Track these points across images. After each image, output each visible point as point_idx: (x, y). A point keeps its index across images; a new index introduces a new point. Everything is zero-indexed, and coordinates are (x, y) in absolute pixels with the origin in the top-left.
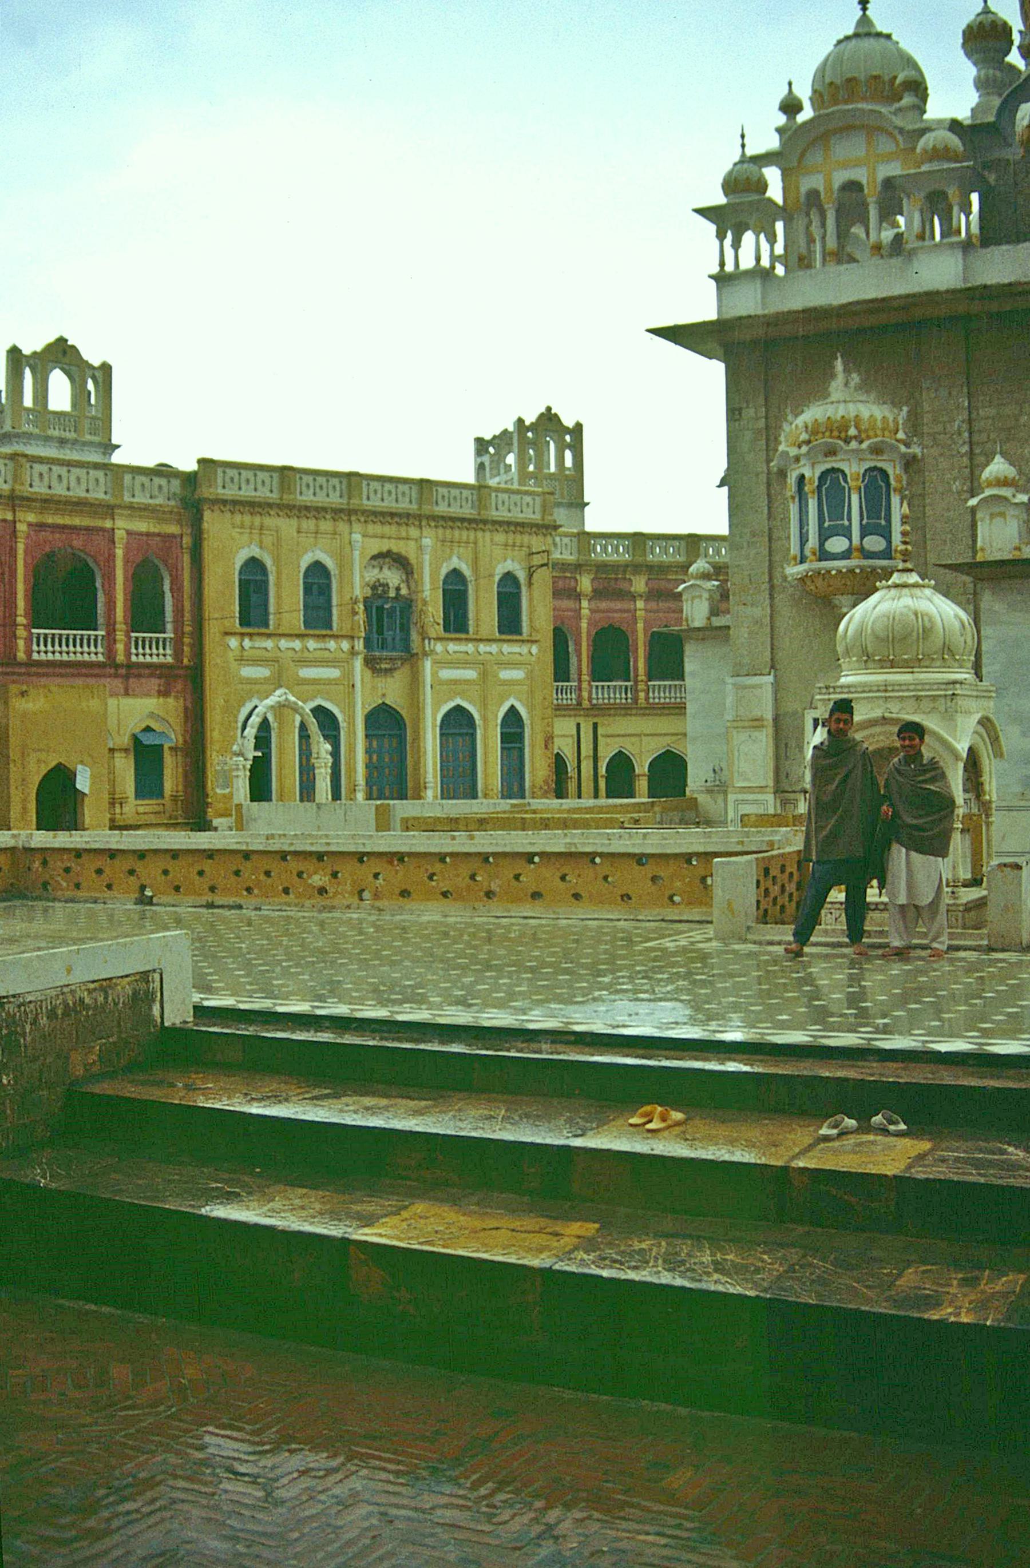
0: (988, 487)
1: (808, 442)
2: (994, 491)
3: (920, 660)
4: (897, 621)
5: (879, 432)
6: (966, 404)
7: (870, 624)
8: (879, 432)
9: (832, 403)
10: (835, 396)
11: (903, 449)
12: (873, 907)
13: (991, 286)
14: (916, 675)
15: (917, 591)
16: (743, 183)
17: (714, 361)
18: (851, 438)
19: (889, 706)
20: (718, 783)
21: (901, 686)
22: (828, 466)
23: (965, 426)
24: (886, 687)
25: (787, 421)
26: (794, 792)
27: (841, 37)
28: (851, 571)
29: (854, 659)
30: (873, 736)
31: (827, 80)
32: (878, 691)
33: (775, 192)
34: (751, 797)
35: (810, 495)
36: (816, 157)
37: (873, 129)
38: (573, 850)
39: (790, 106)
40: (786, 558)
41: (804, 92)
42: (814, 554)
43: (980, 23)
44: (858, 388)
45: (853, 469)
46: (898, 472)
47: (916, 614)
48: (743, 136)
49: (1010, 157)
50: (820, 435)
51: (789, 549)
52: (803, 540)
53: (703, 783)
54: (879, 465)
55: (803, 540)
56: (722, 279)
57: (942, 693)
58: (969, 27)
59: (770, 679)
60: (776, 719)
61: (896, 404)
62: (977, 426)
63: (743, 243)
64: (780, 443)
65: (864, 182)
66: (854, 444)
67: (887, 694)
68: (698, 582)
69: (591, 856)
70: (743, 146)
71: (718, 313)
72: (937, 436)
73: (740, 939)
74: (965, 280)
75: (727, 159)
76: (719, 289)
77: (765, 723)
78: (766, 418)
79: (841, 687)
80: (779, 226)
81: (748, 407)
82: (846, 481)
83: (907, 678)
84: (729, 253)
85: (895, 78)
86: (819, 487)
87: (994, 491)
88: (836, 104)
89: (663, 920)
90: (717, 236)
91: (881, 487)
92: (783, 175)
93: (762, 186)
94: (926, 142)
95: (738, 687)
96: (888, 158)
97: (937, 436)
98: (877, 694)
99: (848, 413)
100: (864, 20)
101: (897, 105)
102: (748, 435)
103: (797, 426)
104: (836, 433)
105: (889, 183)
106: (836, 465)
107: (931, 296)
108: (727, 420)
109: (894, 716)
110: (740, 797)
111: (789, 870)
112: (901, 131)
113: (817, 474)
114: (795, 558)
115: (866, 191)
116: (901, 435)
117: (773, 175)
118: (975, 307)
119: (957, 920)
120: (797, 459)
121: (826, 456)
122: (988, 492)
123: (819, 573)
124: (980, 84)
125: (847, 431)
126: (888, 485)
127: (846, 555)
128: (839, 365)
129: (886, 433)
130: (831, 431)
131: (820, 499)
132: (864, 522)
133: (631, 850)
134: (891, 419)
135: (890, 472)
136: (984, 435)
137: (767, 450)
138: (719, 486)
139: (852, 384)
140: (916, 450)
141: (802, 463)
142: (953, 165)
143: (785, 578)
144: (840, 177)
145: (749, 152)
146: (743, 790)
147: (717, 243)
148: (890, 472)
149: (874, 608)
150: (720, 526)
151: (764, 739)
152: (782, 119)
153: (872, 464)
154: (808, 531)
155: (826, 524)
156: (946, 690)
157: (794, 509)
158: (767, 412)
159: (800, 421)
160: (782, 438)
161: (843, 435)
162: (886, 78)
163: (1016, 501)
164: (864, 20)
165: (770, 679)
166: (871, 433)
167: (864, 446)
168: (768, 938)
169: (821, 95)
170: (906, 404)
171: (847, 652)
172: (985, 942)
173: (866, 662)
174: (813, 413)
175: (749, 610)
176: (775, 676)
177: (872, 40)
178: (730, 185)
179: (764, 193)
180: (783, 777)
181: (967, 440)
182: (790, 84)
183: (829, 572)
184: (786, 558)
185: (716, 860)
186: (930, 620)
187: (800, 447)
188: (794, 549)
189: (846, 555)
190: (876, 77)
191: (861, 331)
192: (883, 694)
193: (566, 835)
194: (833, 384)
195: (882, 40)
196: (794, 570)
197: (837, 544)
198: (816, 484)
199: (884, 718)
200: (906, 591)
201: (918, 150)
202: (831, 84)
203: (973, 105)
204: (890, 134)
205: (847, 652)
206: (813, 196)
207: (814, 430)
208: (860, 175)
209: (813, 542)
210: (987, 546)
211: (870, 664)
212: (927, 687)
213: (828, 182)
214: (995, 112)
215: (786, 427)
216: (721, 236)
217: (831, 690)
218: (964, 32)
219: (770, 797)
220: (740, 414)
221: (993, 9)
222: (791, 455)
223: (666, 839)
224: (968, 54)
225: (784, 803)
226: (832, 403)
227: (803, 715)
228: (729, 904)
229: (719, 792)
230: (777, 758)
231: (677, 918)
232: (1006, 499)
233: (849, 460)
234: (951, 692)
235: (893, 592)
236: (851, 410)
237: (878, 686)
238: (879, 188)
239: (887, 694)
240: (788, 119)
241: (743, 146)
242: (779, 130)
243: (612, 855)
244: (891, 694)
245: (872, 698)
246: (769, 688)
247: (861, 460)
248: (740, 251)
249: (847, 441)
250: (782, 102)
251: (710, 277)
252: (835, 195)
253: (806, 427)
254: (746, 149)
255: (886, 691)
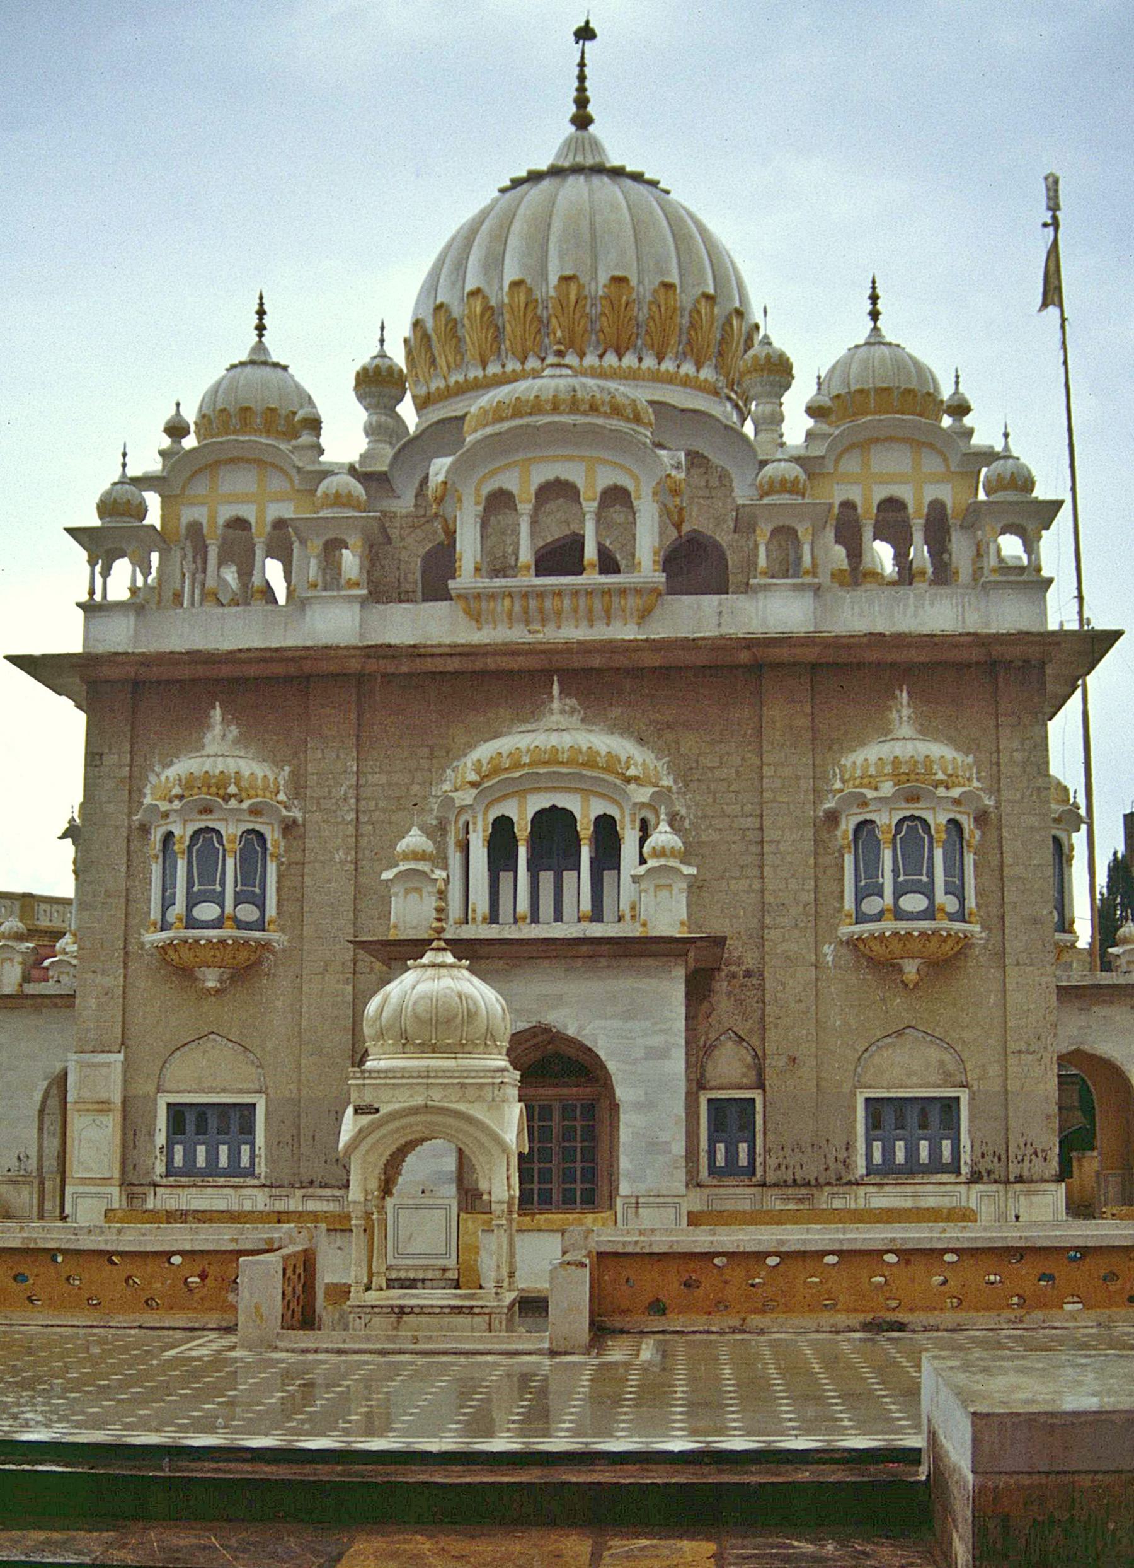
0: (402, 860)
1: (181, 797)
2: (412, 865)
3: (463, 1045)
4: (440, 1003)
5: (260, 792)
6: (355, 769)
7: (411, 1003)
8: (260, 792)
9: (208, 756)
10: (209, 750)
11: (284, 812)
12: (409, 1310)
13: (395, 646)
14: (460, 1061)
15: (455, 971)
16: (120, 506)
17: (64, 698)
18: (230, 796)
19: (430, 1093)
20: (22, 1173)
21: (445, 1073)
22: (202, 825)
23: (352, 793)
24: (427, 1073)
25: (153, 771)
26: (142, 1185)
27: (236, 362)
28: (222, 942)
29: (390, 1042)
30: (411, 1126)
31: (219, 406)
32: (419, 1077)
33: (154, 517)
34: (93, 1189)
35: (179, 855)
36: (201, 488)
37: (262, 463)
38: (32, 1246)
39: (176, 430)
40: (145, 924)
41: (190, 415)
42: (180, 920)
43: (377, 366)
44: (236, 742)
45: (231, 830)
46: (276, 837)
47: (460, 997)
48: (124, 455)
49: (398, 510)
50: (196, 790)
51: (149, 913)
52: (167, 903)
53: (5, 1173)
54: (258, 827)
55: (167, 903)
56: (89, 608)
57: (490, 1080)
58: (365, 370)
59: (121, 1056)
60: (125, 1101)
61: (278, 764)
62: (365, 793)
63: (112, 572)
64: (145, 795)
65: (253, 521)
66: (233, 803)
67: (430, 1081)
68: (10, 943)
69: (52, 1253)
70: (124, 465)
71: (84, 646)
72: (322, 801)
73: (270, 1346)
74: (362, 636)
75: (106, 477)
76: (86, 618)
77: (112, 1106)
78: (131, 766)
79: (370, 1072)
80: (155, 557)
81: (110, 752)
82: (221, 843)
83: (451, 1063)
84: (99, 580)
85: (295, 413)
86: (190, 847)
87: (412, 865)
88: (227, 434)
89: (140, 1327)
90: (89, 562)
91: (256, 852)
92: (162, 502)
93: (142, 511)
94: (328, 485)
95: (83, 1065)
96: (279, 498)
97: (322, 801)
98: (420, 1081)
99: (228, 767)
100: (260, 347)
101: (294, 443)
102: (110, 784)
103: (167, 778)
104: (213, 790)
105: (280, 524)
106: (211, 825)
107: (327, 651)
108: (86, 765)
109: (437, 1104)
110: (80, 1189)
111: (298, 1271)
112: (299, 470)
113: (189, 832)
114: (155, 924)
115: (253, 531)
116: (282, 797)
117: (153, 500)
118: (372, 666)
119: (501, 1323)
120: (166, 815)
121: (200, 812)
122: (403, 867)
123: (186, 942)
124: (371, 430)
125: (226, 789)
126: (265, 849)
127: (218, 924)
128: (217, 714)
129: (268, 794)
130: (209, 787)
131: (190, 863)
132: (238, 889)
133: (103, 1247)
134: (272, 779)
135: (268, 836)
136: (372, 805)
137: (129, 802)
138: (60, 838)
139: (230, 737)
140: (297, 814)
141: (171, 819)
142: (356, 514)
143: (142, 946)
144: (226, 513)
145: (132, 472)
146: (84, 1181)
147: (88, 568)
148: (269, 837)
149: (414, 987)
150: (64, 886)
151: (111, 1123)
152: (166, 442)
153: (250, 826)
154: (174, 894)
155: (195, 889)
156: (493, 1078)
157: (156, 869)
158: (132, 760)
159: (171, 772)
160: (148, 790)
161: (221, 792)
162: (284, 412)
163: (434, 876)
164: (260, 347)
165: (121, 1056)
166: (252, 793)
167: (245, 805)
168: (303, 1345)
169: (210, 422)
170: (289, 763)
171: (381, 1035)
172: (547, 1345)
173: (404, 1045)
174: (184, 766)
175: (99, 979)
176: (126, 1054)
177: (268, 369)
178: (106, 507)
179: (144, 519)
180: (130, 1168)
181: (354, 807)
182: (178, 405)
183: (197, 941)
184: (145, 924)
185: (242, 1259)
186: (475, 1004)
187: (171, 802)
188: (155, 914)
189: (218, 924)
190: (272, 410)
191: (195, 681)
192: (425, 1081)
193: (22, 1228)
194: (209, 736)
195: (280, 371)
196: (154, 937)
197: (207, 911)
198: (187, 843)
199: (426, 1106)
200: (443, 971)
201: (319, 493)
202: (223, 410)
203: (362, 451)
204: (285, 473)
205: (381, 1035)
206: (195, 529)
207: (189, 783)
208: (249, 512)
209: (179, 907)
210: (401, 924)
211: (409, 1048)
212: (473, 1074)
213: (213, 518)
214: (388, 461)
215: (153, 778)
216: (92, 563)
217: (367, 1075)
218: (358, 374)
219: (115, 1191)
220: (101, 759)
221: (389, 354)
222: (162, 809)
223: (144, 1235)
224: (360, 398)
225: (131, 1197)
226: (208, 756)
227: (156, 1100)
228: (257, 1307)
229: (24, 1183)
230: (124, 1146)
231: (158, 1325)
232: (424, 873)
233: (226, 820)
234: (499, 1080)
235: (431, 972)
236: (231, 765)
237: (419, 1071)
238: (268, 529)
239: (430, 1081)
240: (173, 442)
241: (124, 465)
242: (162, 453)
243: (78, 1252)
244: (433, 1081)
245: (394, 1084)
246: (119, 1068)
247: (239, 820)
248: (109, 579)
249: (227, 798)
250: (168, 423)
251: (79, 605)
252: (219, 532)
253: (180, 780)
254: (127, 469)
255: (428, 1077)
